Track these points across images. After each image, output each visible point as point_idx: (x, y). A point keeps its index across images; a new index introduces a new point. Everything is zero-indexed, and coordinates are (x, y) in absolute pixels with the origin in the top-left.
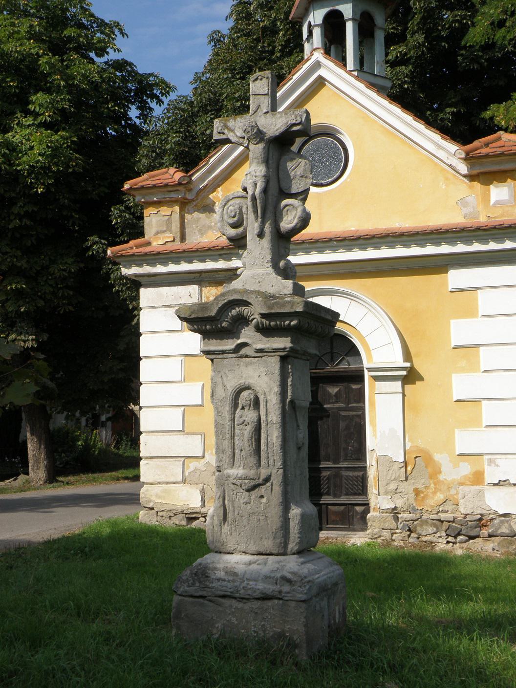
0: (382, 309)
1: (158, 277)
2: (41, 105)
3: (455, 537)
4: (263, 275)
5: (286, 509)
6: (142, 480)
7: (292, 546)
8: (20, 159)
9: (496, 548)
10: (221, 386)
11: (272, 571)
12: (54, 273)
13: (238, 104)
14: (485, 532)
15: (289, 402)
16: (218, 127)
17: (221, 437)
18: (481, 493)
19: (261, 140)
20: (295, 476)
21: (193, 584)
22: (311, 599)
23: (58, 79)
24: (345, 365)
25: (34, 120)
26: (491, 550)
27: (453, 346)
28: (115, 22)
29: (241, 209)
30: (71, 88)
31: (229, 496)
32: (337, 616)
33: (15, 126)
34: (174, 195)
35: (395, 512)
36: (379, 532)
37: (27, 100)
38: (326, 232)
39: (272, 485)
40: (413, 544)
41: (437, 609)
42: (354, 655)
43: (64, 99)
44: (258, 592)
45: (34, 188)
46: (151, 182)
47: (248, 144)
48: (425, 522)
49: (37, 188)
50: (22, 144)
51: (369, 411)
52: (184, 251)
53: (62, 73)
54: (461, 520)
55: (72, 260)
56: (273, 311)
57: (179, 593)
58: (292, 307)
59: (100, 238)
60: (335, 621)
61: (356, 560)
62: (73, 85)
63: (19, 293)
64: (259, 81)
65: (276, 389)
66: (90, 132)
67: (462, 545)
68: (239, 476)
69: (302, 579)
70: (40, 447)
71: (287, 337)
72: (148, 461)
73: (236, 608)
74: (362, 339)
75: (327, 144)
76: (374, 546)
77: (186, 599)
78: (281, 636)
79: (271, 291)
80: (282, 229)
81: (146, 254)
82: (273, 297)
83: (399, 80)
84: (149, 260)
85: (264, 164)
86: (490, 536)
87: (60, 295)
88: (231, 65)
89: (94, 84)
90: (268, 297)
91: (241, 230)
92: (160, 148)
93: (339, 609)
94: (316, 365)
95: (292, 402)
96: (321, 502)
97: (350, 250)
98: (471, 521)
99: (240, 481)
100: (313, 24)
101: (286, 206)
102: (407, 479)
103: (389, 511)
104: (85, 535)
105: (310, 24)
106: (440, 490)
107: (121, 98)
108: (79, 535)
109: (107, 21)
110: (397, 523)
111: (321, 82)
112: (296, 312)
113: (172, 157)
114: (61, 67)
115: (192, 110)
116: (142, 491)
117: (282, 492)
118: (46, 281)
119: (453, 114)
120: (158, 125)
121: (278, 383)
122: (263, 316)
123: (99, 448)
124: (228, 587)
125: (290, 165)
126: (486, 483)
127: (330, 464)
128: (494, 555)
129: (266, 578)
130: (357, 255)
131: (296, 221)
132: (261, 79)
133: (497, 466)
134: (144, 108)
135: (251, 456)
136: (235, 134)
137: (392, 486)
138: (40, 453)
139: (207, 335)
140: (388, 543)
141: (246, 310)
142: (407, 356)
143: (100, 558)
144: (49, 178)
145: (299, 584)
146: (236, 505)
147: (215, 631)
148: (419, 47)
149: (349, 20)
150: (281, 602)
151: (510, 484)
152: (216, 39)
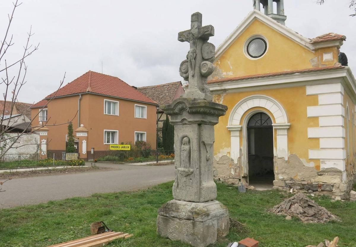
3: (307, 191)
39: (194, 175)
91: (187, 74)
101: (203, 64)
133: (326, 164)
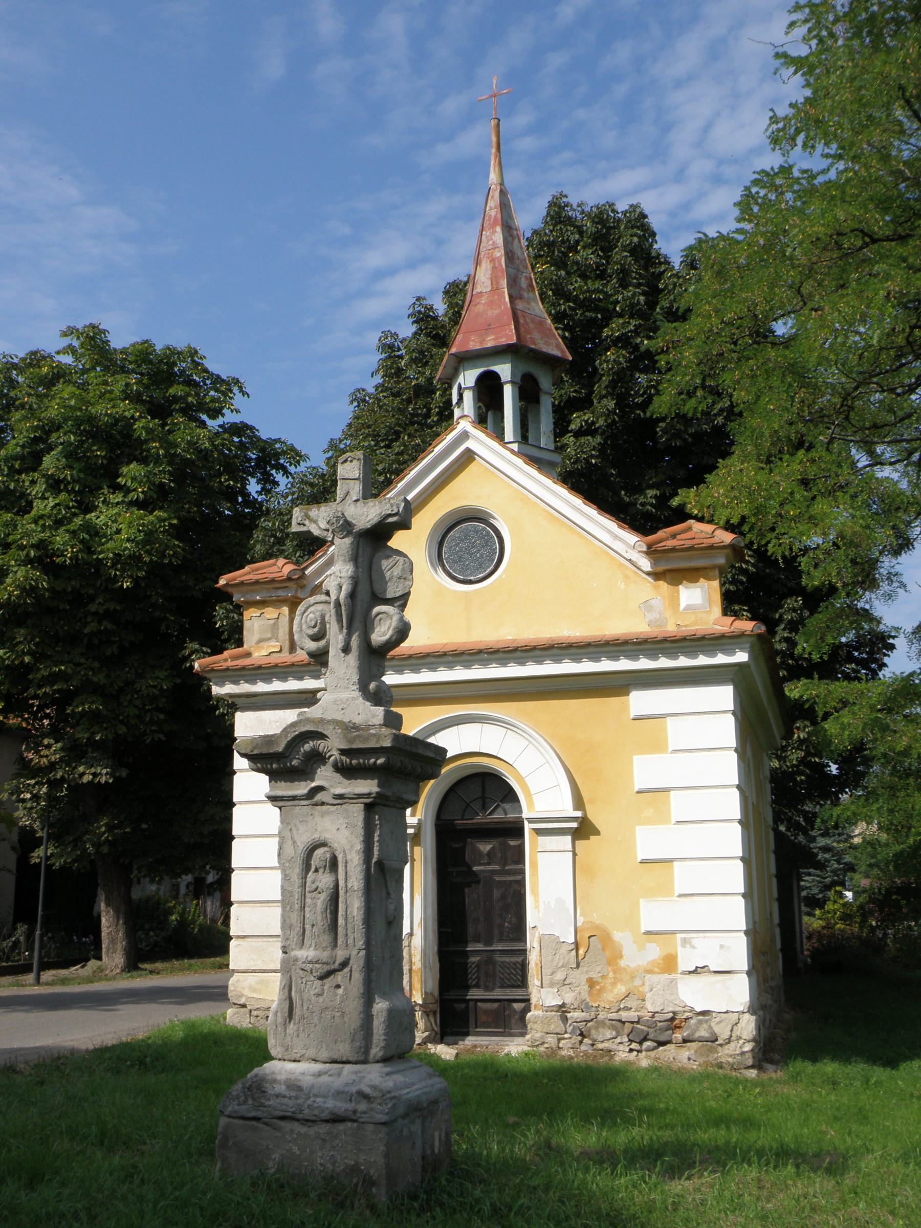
0: (546, 740)
1: (264, 697)
2: (134, 479)
4: (347, 700)
5: (368, 1002)
6: (231, 967)
7: (376, 1051)
8: (103, 544)
9: (693, 1057)
10: (290, 843)
11: (347, 1085)
12: (140, 690)
13: (382, 478)
14: (678, 1036)
15: (376, 862)
16: (297, 518)
17: (288, 909)
18: (672, 984)
19: (349, 533)
20: (383, 960)
21: (245, 1102)
22: (395, 1120)
23: (156, 447)
24: (501, 814)
25: (124, 496)
26: (686, 1061)
27: (636, 790)
28: (233, 379)
29: (323, 617)
30: (171, 458)
31: (296, 986)
32: (437, 1143)
33: (101, 505)
34: (281, 593)
35: (562, 1009)
36: (542, 1037)
37: (118, 472)
38: (475, 642)
39: (351, 971)
40: (585, 1053)
41: (581, 1138)
42: (450, 1195)
43: (163, 471)
44: (327, 1112)
45: (118, 582)
46: (253, 577)
47: (333, 538)
48: (602, 1024)
49: (122, 582)
50: (107, 526)
51: (530, 876)
52: (293, 665)
53: (160, 440)
54: (648, 1020)
55: (166, 674)
56: (354, 746)
57: (227, 1113)
58: (377, 741)
59: (202, 645)
60: (433, 1151)
61: (507, 1076)
62: (175, 454)
63: (94, 717)
64: (348, 463)
65: (359, 846)
66: (194, 512)
67: (649, 1053)
68: (309, 958)
69: (383, 1096)
70: (118, 923)
71: (372, 779)
72: (240, 942)
73: (299, 1133)
74: (521, 780)
75: (477, 532)
76: (534, 1056)
77: (236, 1121)
78: (354, 1169)
79: (358, 720)
80: (373, 643)
81: (243, 668)
82: (356, 727)
83: (583, 452)
84: (248, 675)
85: (351, 563)
86: (685, 1041)
87: (148, 719)
88: (374, 430)
89: (204, 453)
90: (349, 728)
91: (322, 643)
92: (282, 531)
93: (440, 1135)
94: (463, 815)
95: (380, 863)
96: (468, 997)
97: (540, 662)
98: (660, 1022)
99: (311, 966)
100: (463, 386)
101: (378, 614)
102: (578, 966)
103: (555, 1009)
104: (150, 1041)
105: (460, 387)
106: (621, 980)
107: (236, 469)
108: (143, 1040)
109: (224, 377)
110: (565, 1025)
111: (469, 457)
112: (382, 748)
113: (295, 543)
114: (162, 432)
115: (323, 484)
116: (231, 982)
117: (364, 980)
118: (130, 701)
119: (655, 497)
120: (282, 502)
121: (362, 839)
122: (343, 752)
123: (200, 925)
124: (289, 1106)
125: (385, 564)
126: (680, 971)
127: (480, 947)
128: (690, 1066)
129: (339, 1094)
130: (549, 668)
131: (390, 633)
132: (351, 461)
134: (268, 482)
135: (324, 932)
136: (318, 525)
137: (560, 976)
138: (117, 931)
139: (274, 776)
140: (553, 1052)
141: (321, 745)
142: (579, 803)
143: (163, 1071)
144: (139, 569)
145: (379, 1101)
146: (305, 997)
147: (271, 1164)
148: (609, 415)
149: (507, 382)
150: (355, 1125)
151: (710, 972)
152: (359, 398)
